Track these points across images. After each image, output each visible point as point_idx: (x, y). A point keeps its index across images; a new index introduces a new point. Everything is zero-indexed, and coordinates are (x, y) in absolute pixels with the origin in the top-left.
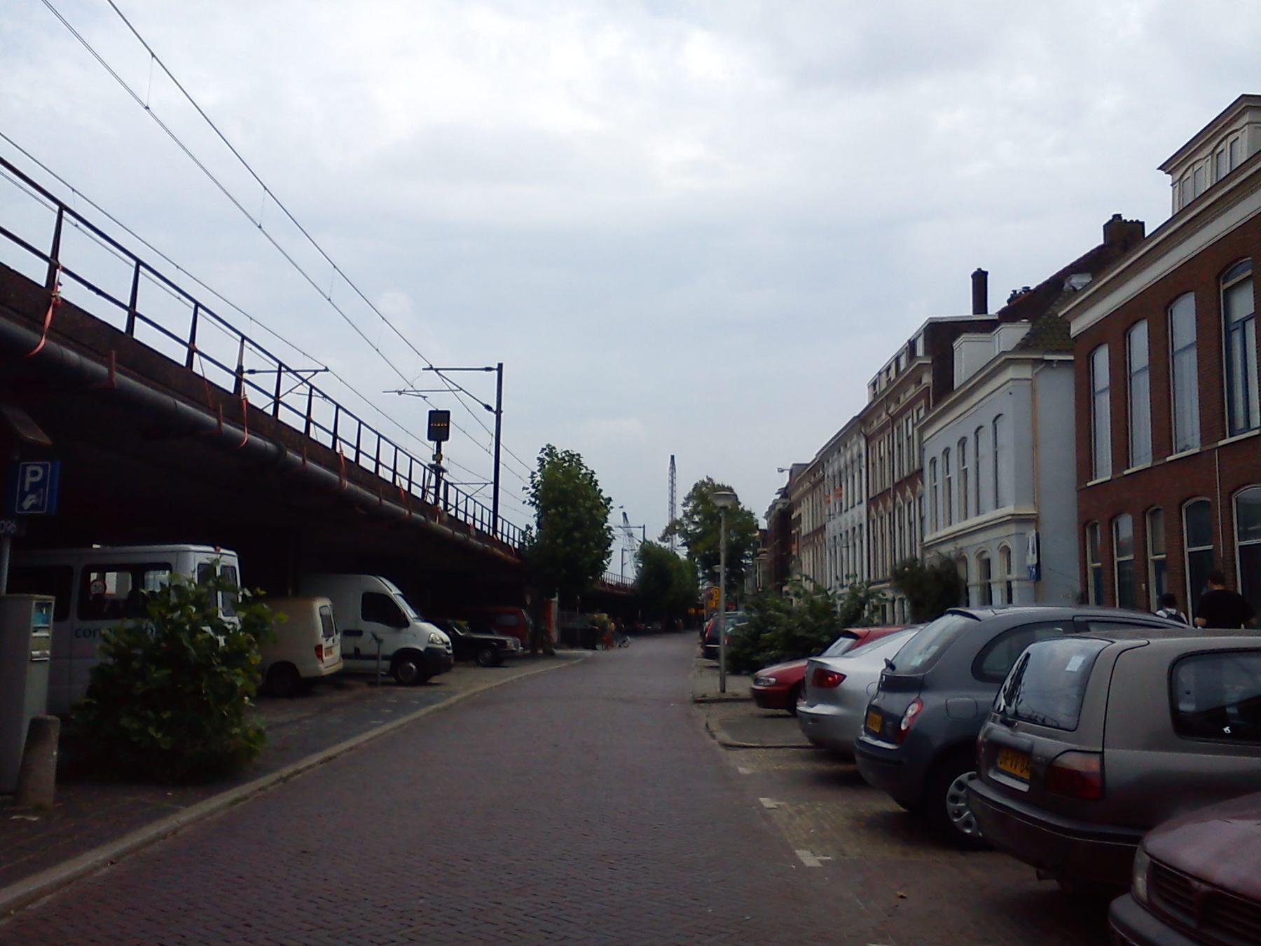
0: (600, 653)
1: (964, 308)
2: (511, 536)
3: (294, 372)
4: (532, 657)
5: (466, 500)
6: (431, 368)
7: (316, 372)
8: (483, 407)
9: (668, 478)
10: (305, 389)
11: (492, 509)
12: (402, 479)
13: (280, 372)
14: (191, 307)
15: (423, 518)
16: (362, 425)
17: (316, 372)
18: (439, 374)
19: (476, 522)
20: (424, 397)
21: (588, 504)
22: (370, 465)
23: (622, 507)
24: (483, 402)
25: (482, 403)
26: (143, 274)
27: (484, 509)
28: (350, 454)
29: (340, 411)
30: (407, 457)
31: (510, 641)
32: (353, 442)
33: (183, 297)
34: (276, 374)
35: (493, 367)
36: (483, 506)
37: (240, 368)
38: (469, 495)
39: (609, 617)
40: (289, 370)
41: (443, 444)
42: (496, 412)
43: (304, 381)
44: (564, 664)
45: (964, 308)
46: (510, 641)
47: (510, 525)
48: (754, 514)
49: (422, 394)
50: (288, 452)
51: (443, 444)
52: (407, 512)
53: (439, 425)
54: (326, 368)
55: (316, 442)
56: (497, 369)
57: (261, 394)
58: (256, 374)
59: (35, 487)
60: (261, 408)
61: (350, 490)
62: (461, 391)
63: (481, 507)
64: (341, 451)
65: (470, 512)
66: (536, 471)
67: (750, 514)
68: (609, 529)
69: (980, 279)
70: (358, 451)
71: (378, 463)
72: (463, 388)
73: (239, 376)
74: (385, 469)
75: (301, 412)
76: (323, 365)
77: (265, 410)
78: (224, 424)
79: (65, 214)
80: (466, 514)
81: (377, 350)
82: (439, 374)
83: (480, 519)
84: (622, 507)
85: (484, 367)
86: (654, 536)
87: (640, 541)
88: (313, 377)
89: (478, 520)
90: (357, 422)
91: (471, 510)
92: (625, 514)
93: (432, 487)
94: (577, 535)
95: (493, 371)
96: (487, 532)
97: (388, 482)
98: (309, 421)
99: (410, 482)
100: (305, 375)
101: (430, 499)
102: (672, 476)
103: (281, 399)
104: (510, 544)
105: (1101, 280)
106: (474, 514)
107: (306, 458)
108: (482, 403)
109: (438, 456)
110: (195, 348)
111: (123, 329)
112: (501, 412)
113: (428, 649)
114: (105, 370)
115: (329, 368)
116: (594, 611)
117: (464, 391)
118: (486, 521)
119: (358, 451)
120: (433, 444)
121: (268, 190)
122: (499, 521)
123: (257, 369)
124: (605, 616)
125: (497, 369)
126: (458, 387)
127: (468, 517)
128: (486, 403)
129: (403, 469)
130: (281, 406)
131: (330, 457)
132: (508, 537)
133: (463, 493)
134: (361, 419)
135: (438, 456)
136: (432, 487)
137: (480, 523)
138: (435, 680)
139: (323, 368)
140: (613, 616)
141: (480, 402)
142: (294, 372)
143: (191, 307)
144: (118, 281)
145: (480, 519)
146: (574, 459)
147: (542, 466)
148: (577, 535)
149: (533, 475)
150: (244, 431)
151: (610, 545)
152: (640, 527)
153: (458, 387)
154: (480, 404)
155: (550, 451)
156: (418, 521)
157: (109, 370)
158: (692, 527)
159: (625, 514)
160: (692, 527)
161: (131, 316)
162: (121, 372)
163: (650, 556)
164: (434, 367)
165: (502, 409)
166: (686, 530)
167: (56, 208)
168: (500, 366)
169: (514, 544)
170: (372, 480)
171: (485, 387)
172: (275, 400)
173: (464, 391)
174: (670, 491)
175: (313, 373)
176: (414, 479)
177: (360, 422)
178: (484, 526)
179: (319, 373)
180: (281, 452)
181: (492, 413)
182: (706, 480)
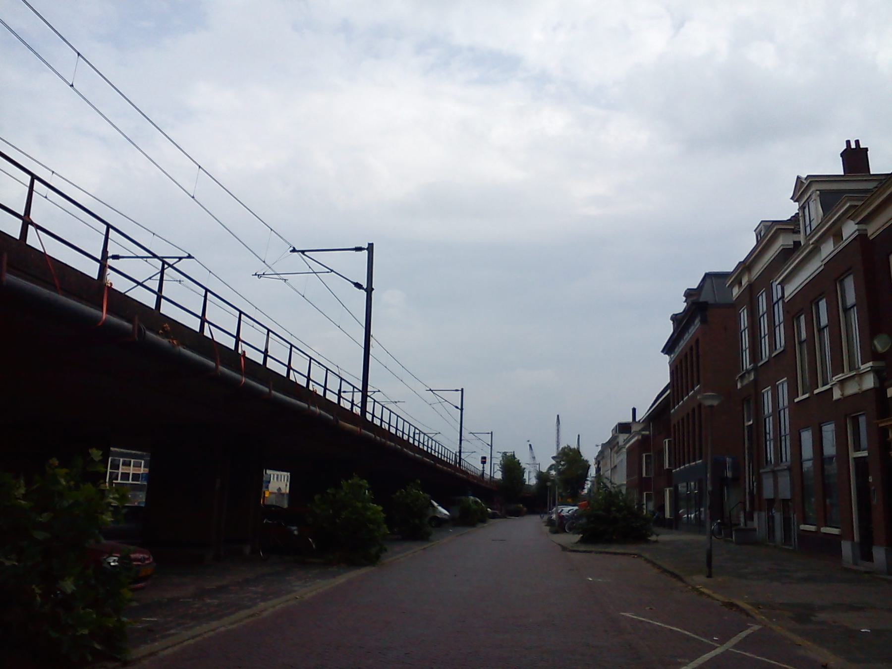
1: (629, 419)
5: (163, 269)
7: (180, 258)
9: (555, 428)
12: (385, 424)
14: (287, 348)
16: (392, 413)
17: (180, 258)
18: (434, 393)
19: (415, 441)
22: (334, 399)
23: (529, 441)
24: (352, 280)
25: (454, 406)
26: (294, 352)
29: (343, 382)
33: (321, 366)
34: (351, 393)
37: (340, 391)
41: (485, 465)
42: (366, 290)
45: (629, 419)
52: (359, 429)
54: (189, 254)
56: (367, 249)
57: (252, 349)
58: (121, 259)
62: (332, 273)
63: (408, 425)
64: (356, 411)
67: (587, 461)
69: (634, 410)
70: (325, 389)
72: (334, 270)
73: (160, 294)
74: (345, 401)
76: (186, 252)
78: (362, 430)
79: (328, 371)
80: (397, 429)
82: (434, 393)
84: (529, 441)
85: (455, 389)
86: (544, 469)
89: (417, 440)
90: (238, 313)
92: (530, 445)
93: (417, 434)
95: (363, 251)
96: (401, 436)
99: (382, 420)
100: (170, 261)
101: (357, 410)
103: (269, 354)
105: (749, 355)
106: (424, 442)
108: (454, 406)
109: (483, 468)
110: (30, 219)
111: (198, 330)
115: (192, 255)
119: (325, 389)
124: (521, 505)
125: (367, 249)
127: (404, 435)
128: (356, 282)
129: (378, 414)
130: (268, 358)
131: (260, 371)
132: (450, 459)
133: (387, 409)
134: (292, 343)
135: (483, 468)
136: (417, 434)
139: (186, 255)
143: (287, 348)
144: (146, 270)
145: (371, 412)
147: (503, 458)
149: (500, 461)
150: (102, 311)
152: (489, 433)
154: (350, 283)
156: (417, 458)
159: (530, 445)
163: (541, 476)
164: (297, 249)
165: (373, 287)
167: (325, 369)
169: (438, 456)
170: (322, 401)
171: (456, 398)
175: (178, 260)
176: (350, 400)
181: (363, 291)
182: (566, 446)
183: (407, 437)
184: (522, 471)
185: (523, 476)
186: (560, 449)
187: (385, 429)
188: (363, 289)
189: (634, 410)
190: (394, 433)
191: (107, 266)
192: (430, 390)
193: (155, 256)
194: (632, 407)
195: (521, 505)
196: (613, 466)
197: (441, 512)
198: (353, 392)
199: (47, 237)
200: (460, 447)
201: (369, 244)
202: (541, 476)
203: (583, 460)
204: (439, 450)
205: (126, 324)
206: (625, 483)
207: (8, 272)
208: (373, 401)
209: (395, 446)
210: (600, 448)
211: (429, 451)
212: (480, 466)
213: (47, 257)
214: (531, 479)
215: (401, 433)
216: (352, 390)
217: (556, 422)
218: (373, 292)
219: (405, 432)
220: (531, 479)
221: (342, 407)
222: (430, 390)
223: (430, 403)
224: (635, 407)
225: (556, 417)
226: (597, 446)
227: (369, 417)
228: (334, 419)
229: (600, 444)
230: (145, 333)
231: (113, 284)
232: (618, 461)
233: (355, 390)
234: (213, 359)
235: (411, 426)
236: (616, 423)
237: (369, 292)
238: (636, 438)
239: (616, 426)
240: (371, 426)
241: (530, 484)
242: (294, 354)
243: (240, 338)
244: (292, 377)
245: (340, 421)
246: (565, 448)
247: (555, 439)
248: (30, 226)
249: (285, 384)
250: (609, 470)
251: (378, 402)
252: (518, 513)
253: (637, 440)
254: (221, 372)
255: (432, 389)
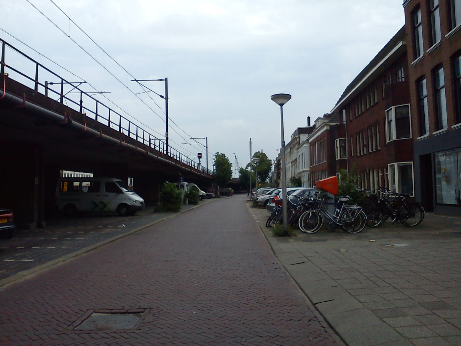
0: (230, 197)
1: (306, 125)
2: (192, 164)
3: (70, 84)
4: (215, 197)
6: (192, 138)
7: (81, 83)
8: (159, 97)
9: (249, 145)
10: (163, 143)
11: (206, 168)
13: (62, 83)
15: (175, 164)
16: (138, 128)
17: (81, 83)
18: (194, 140)
20: (191, 145)
21: (227, 165)
22: (134, 137)
23: (234, 154)
24: (159, 94)
27: (175, 150)
28: (126, 133)
29: (6, 46)
30: (148, 134)
31: (212, 194)
32: (59, 92)
34: (61, 84)
35: (205, 138)
36: (180, 153)
38: (192, 160)
39: (231, 189)
40: (67, 82)
41: (201, 159)
42: (165, 99)
43: (75, 87)
44: (221, 199)
46: (212, 194)
47: (182, 155)
48: (324, 114)
49: (190, 144)
50: (73, 121)
51: (201, 159)
53: (200, 156)
55: (113, 129)
56: (165, 80)
59: (182, 179)
60: (56, 100)
61: (150, 155)
62: (151, 91)
65: (175, 155)
66: (215, 158)
67: (270, 161)
68: (232, 170)
69: (309, 118)
70: (129, 132)
71: (137, 136)
72: (208, 148)
73: (37, 82)
75: (118, 124)
77: (58, 101)
78: (26, 102)
81: (173, 129)
82: (194, 140)
83: (170, 152)
84: (234, 154)
85: (203, 138)
86: (244, 167)
87: (240, 168)
88: (80, 85)
89: (169, 153)
91: (175, 154)
92: (235, 156)
94: (225, 172)
95: (163, 81)
97: (158, 151)
98: (109, 122)
99: (155, 145)
102: (251, 145)
104: (172, 157)
106: (177, 155)
107: (25, 99)
109: (200, 161)
111: (34, 89)
112: (168, 98)
113: (203, 195)
114: (22, 100)
115: (86, 81)
116: (228, 188)
117: (152, 91)
118: (162, 146)
119: (129, 132)
120: (199, 159)
121: (105, 52)
122: (169, 148)
123: (53, 82)
124: (231, 189)
125: (165, 80)
126: (150, 90)
128: (161, 95)
129: (157, 144)
132: (192, 165)
135: (200, 161)
137: (179, 159)
138: (203, 200)
139: (84, 81)
140: (233, 189)
141: (158, 94)
142: (70, 84)
145: (173, 154)
146: (223, 155)
147: (216, 157)
148: (225, 172)
150: (85, 125)
151: (232, 174)
152: (204, 138)
153: (150, 90)
154: (202, 139)
155: (217, 153)
156: (183, 168)
157: (23, 100)
158: (254, 164)
159: (235, 156)
160: (254, 164)
161: (62, 97)
162: (27, 101)
163: (242, 171)
165: (168, 97)
166: (253, 166)
168: (207, 137)
169: (190, 165)
170: (128, 139)
171: (160, 88)
172: (80, 106)
173: (152, 91)
174: (250, 147)
175: (80, 84)
177: (121, 116)
178: (177, 158)
179: (82, 84)
180: (69, 121)
181: (164, 99)
182: (258, 152)
183: (173, 156)
184: (230, 165)
185: (231, 168)
186: (253, 154)
187: (161, 152)
188: (164, 98)
189: (309, 118)
190: (178, 160)
191: (5, 65)
192: (135, 80)
193: (158, 139)
194: (308, 117)
195: (231, 189)
196: (293, 160)
197: (130, 199)
198: (155, 140)
199: (116, 126)
200: (167, 135)
201: (166, 78)
202: (242, 171)
203: (268, 160)
204: (184, 159)
205: (143, 150)
206: (308, 169)
207: (26, 100)
208: (80, 92)
209: (186, 168)
210: (279, 152)
211: (191, 166)
212: (197, 160)
213: (69, 109)
214: (236, 175)
215: (162, 150)
216: (154, 139)
217: (249, 142)
218: (168, 99)
219: (175, 155)
220: (236, 175)
221: (138, 141)
222: (135, 80)
223: (135, 94)
224: (310, 116)
225: (249, 139)
226: (277, 150)
227: (169, 154)
228: (146, 152)
229: (280, 149)
230: (71, 121)
231: (9, 75)
232: (299, 154)
233: (64, 82)
234: (99, 131)
235: (182, 155)
236: (296, 129)
237: (167, 97)
238: (325, 128)
239: (296, 131)
240: (170, 158)
241: (236, 177)
242: (73, 88)
243: (82, 106)
244: (111, 126)
245: (73, 121)
246: (257, 153)
247: (249, 152)
248: (38, 85)
249: (107, 129)
250: (290, 163)
251: (85, 93)
252: (228, 194)
253: (326, 130)
254: (27, 104)
255: (137, 79)
